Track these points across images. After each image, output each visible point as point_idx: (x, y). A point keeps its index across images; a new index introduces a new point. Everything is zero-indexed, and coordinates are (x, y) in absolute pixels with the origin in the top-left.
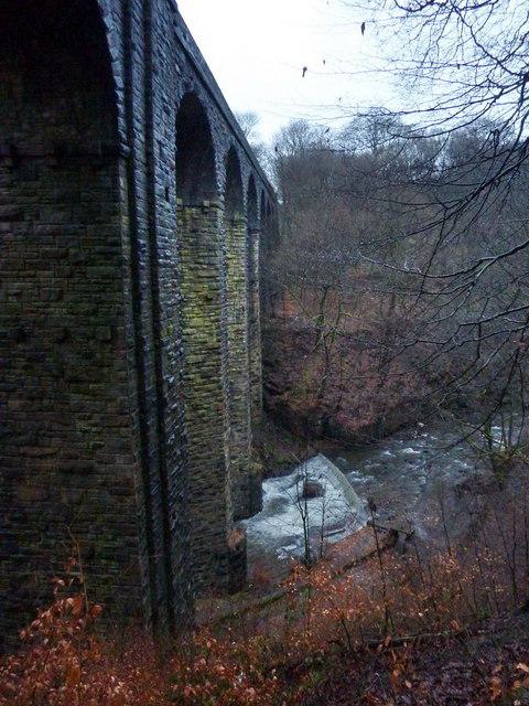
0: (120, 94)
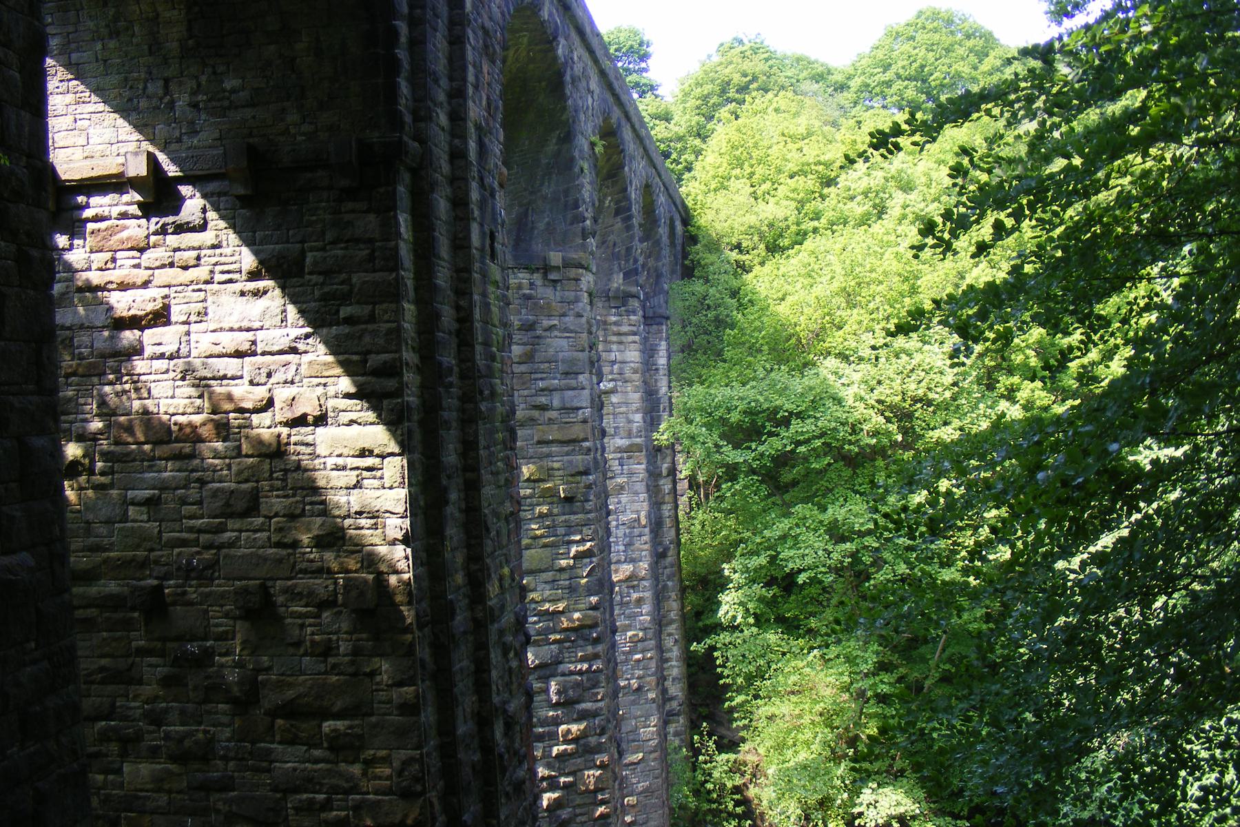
0: (403, 27)
